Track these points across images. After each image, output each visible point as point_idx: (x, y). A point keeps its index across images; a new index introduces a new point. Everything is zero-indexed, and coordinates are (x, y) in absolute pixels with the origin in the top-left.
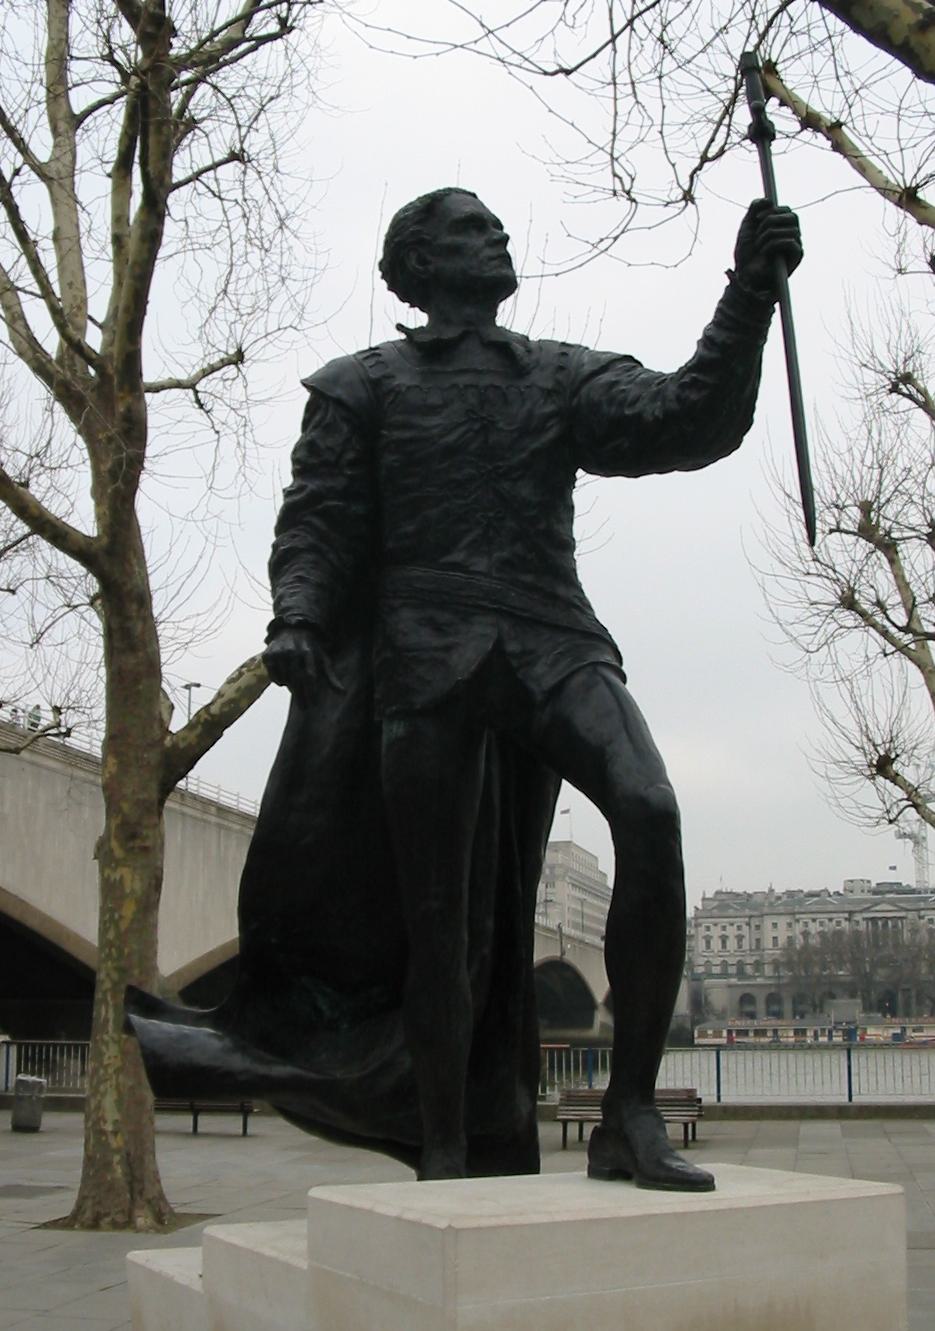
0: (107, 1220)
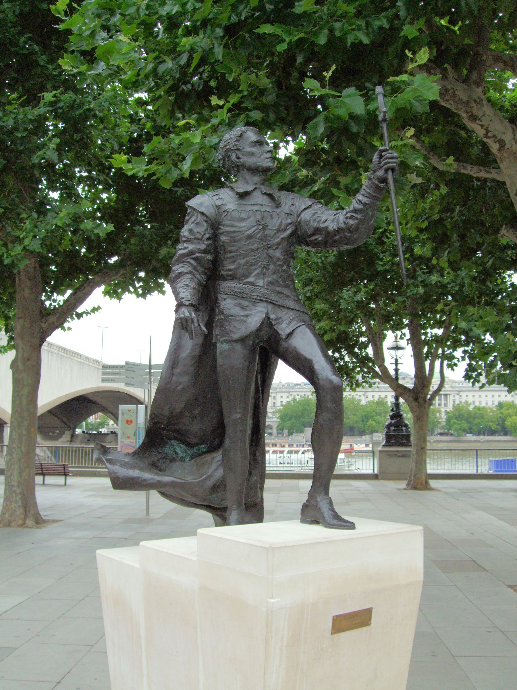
0: (14, 523)
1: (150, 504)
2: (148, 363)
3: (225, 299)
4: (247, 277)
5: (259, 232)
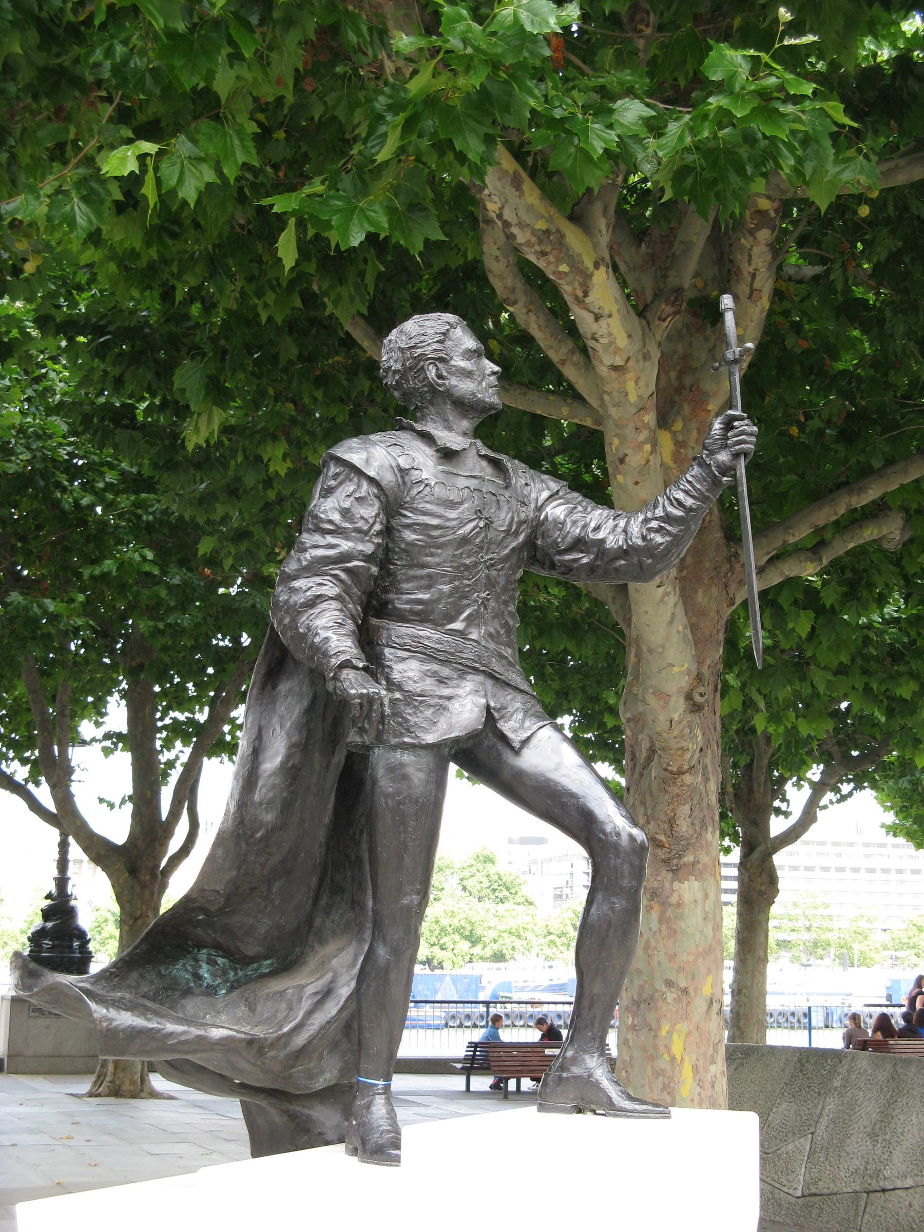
3: (404, 659)
4: (452, 620)
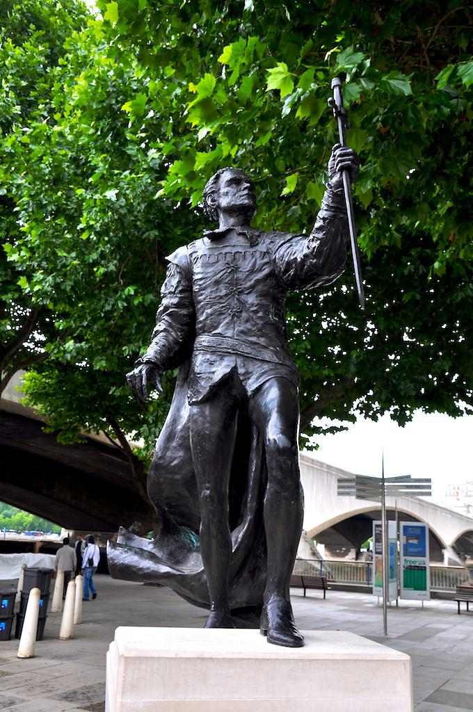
1: (388, 625)
2: (381, 477)
4: (216, 328)
5: (227, 276)
